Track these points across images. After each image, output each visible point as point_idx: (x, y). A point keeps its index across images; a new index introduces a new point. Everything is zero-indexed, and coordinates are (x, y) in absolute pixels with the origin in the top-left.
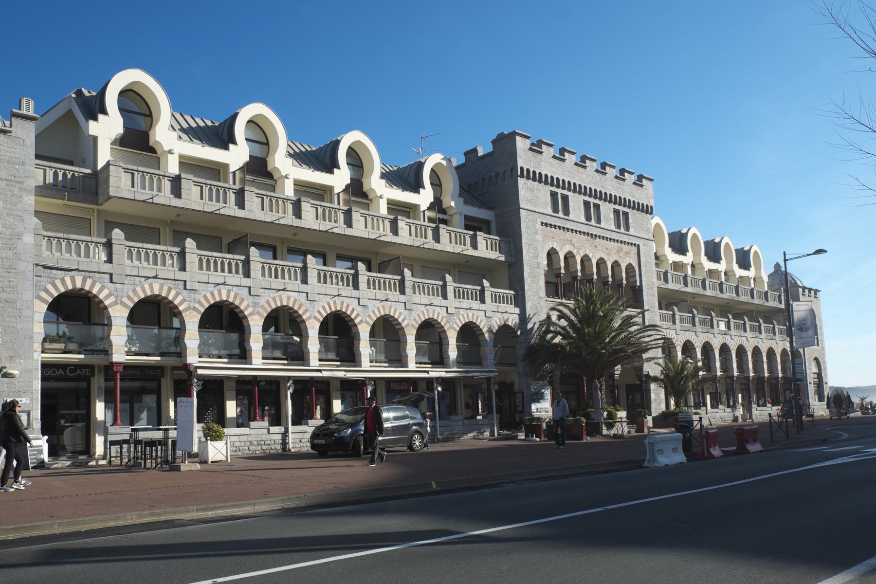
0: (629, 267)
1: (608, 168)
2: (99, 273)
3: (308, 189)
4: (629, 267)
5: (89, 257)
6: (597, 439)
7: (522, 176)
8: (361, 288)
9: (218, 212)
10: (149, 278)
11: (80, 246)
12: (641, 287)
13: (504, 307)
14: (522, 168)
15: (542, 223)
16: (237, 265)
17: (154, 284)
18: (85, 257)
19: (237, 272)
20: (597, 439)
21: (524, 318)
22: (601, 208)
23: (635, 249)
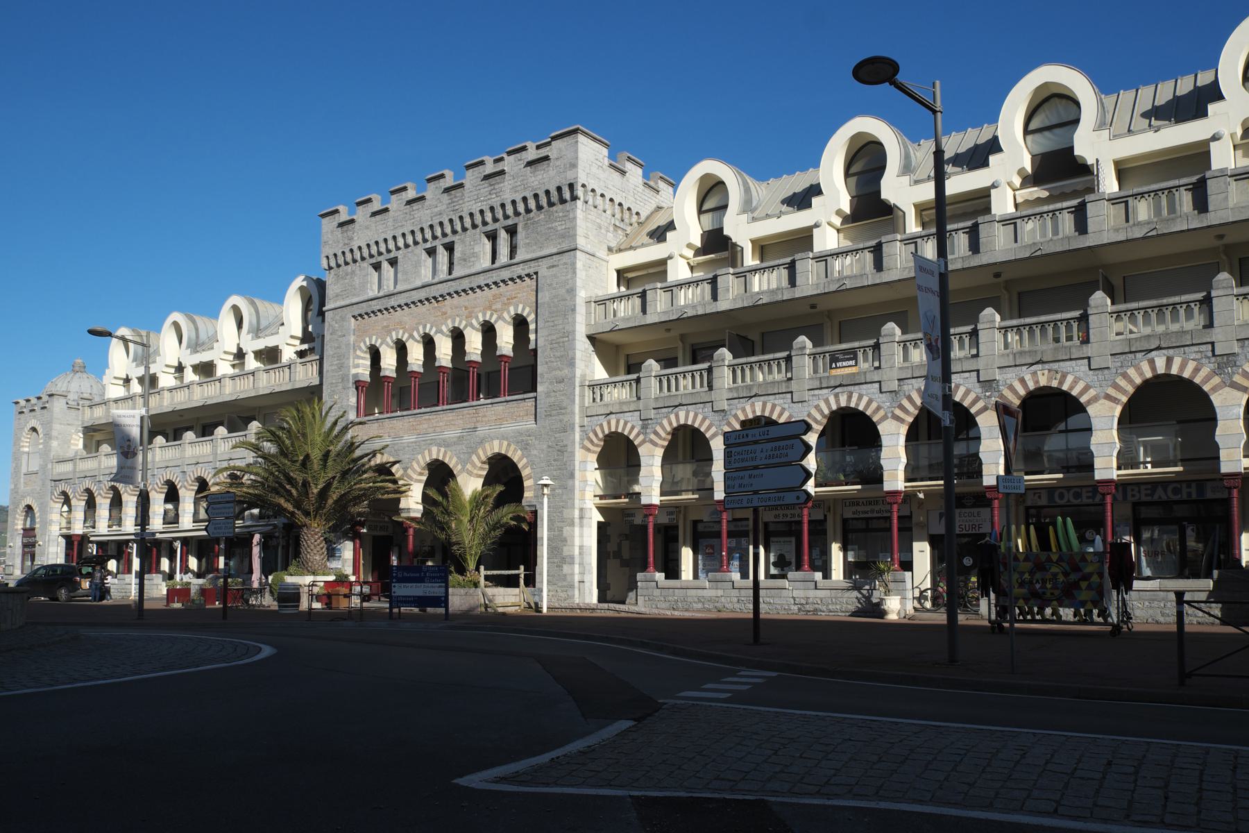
3: (651, 271)
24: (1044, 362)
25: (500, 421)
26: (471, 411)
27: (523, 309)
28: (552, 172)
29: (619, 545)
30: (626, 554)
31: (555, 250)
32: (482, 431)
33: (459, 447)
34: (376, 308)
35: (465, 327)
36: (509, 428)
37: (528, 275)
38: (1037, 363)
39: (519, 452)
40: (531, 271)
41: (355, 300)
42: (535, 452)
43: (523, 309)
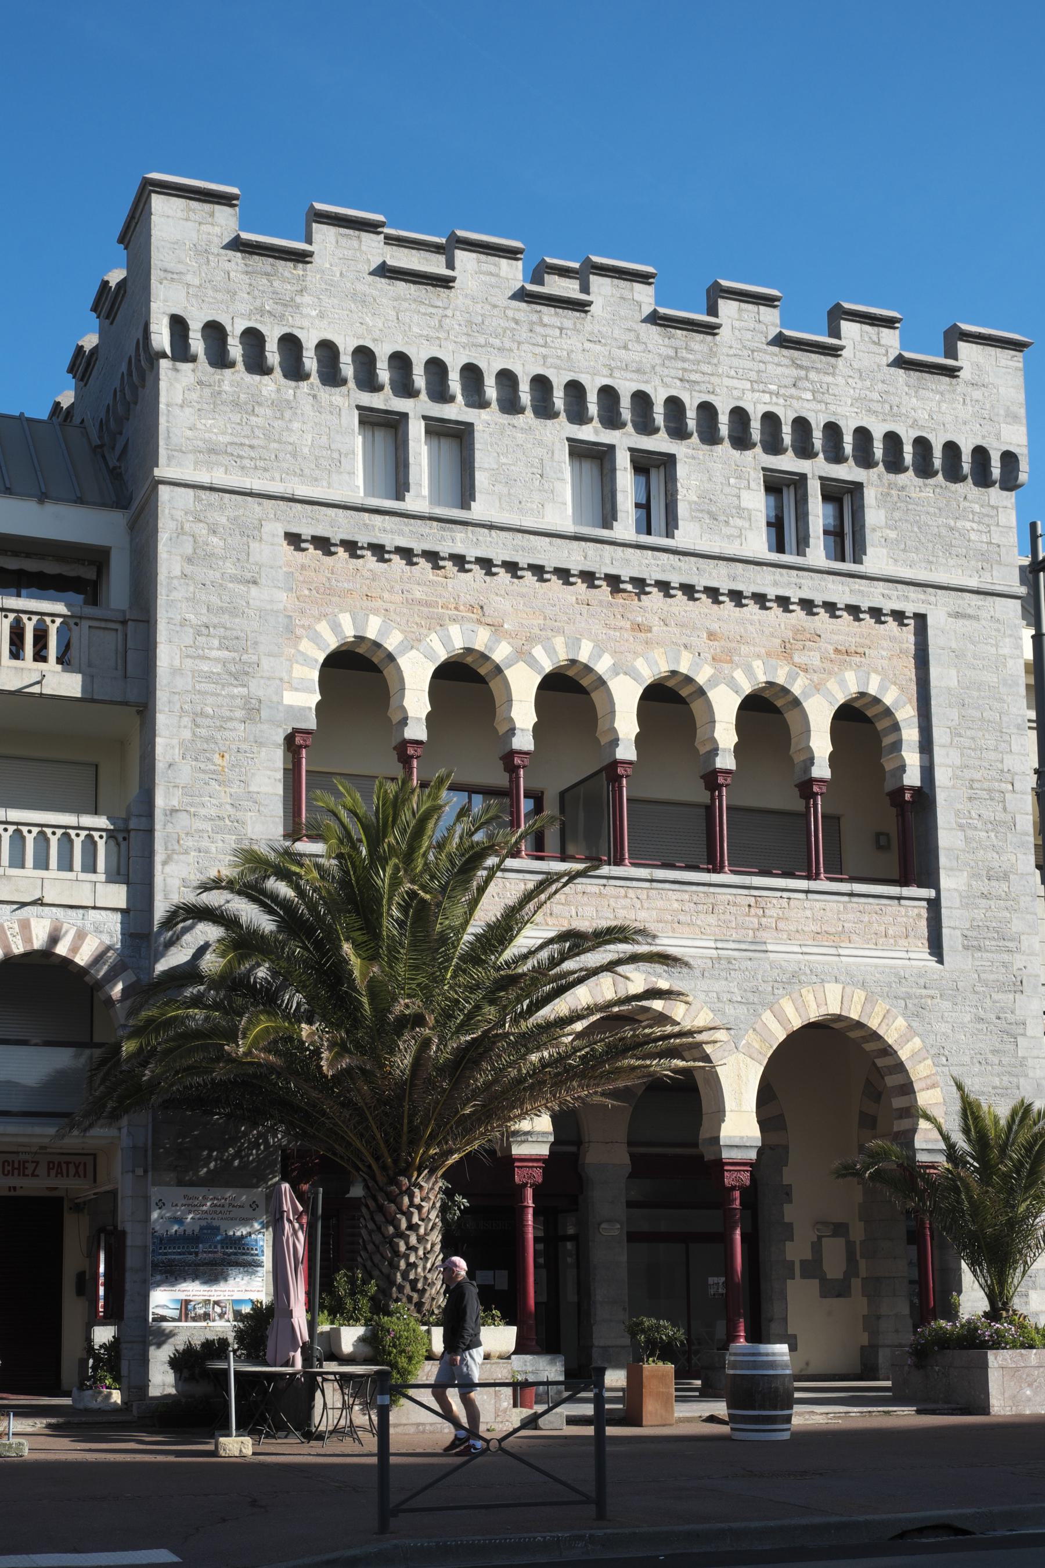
0: (858, 721)
1: (727, 308)
2: (94, 908)
4: (858, 721)
5: (71, 869)
6: (289, 1450)
7: (182, 352)
8: (51, 867)
9: (36, 689)
10: (23, 904)
11: (47, 840)
12: (924, 798)
13: (57, 885)
14: (179, 325)
15: (294, 539)
16: (90, 844)
17: (33, 922)
18: (84, 870)
19: (90, 866)
20: (289, 1450)
21: (141, 932)
22: (681, 471)
23: (908, 636)
24: (42, 904)
25: (839, 937)
26: (743, 898)
27: (336, 627)
28: (573, 342)
29: (817, 1247)
30: (834, 1267)
31: (973, 583)
32: (783, 951)
33: (719, 986)
34: (390, 541)
35: (714, 681)
36: (864, 957)
37: (899, 616)
38: (33, 903)
39: (901, 1022)
40: (910, 609)
41: (303, 491)
42: (944, 1028)
43: (336, 627)
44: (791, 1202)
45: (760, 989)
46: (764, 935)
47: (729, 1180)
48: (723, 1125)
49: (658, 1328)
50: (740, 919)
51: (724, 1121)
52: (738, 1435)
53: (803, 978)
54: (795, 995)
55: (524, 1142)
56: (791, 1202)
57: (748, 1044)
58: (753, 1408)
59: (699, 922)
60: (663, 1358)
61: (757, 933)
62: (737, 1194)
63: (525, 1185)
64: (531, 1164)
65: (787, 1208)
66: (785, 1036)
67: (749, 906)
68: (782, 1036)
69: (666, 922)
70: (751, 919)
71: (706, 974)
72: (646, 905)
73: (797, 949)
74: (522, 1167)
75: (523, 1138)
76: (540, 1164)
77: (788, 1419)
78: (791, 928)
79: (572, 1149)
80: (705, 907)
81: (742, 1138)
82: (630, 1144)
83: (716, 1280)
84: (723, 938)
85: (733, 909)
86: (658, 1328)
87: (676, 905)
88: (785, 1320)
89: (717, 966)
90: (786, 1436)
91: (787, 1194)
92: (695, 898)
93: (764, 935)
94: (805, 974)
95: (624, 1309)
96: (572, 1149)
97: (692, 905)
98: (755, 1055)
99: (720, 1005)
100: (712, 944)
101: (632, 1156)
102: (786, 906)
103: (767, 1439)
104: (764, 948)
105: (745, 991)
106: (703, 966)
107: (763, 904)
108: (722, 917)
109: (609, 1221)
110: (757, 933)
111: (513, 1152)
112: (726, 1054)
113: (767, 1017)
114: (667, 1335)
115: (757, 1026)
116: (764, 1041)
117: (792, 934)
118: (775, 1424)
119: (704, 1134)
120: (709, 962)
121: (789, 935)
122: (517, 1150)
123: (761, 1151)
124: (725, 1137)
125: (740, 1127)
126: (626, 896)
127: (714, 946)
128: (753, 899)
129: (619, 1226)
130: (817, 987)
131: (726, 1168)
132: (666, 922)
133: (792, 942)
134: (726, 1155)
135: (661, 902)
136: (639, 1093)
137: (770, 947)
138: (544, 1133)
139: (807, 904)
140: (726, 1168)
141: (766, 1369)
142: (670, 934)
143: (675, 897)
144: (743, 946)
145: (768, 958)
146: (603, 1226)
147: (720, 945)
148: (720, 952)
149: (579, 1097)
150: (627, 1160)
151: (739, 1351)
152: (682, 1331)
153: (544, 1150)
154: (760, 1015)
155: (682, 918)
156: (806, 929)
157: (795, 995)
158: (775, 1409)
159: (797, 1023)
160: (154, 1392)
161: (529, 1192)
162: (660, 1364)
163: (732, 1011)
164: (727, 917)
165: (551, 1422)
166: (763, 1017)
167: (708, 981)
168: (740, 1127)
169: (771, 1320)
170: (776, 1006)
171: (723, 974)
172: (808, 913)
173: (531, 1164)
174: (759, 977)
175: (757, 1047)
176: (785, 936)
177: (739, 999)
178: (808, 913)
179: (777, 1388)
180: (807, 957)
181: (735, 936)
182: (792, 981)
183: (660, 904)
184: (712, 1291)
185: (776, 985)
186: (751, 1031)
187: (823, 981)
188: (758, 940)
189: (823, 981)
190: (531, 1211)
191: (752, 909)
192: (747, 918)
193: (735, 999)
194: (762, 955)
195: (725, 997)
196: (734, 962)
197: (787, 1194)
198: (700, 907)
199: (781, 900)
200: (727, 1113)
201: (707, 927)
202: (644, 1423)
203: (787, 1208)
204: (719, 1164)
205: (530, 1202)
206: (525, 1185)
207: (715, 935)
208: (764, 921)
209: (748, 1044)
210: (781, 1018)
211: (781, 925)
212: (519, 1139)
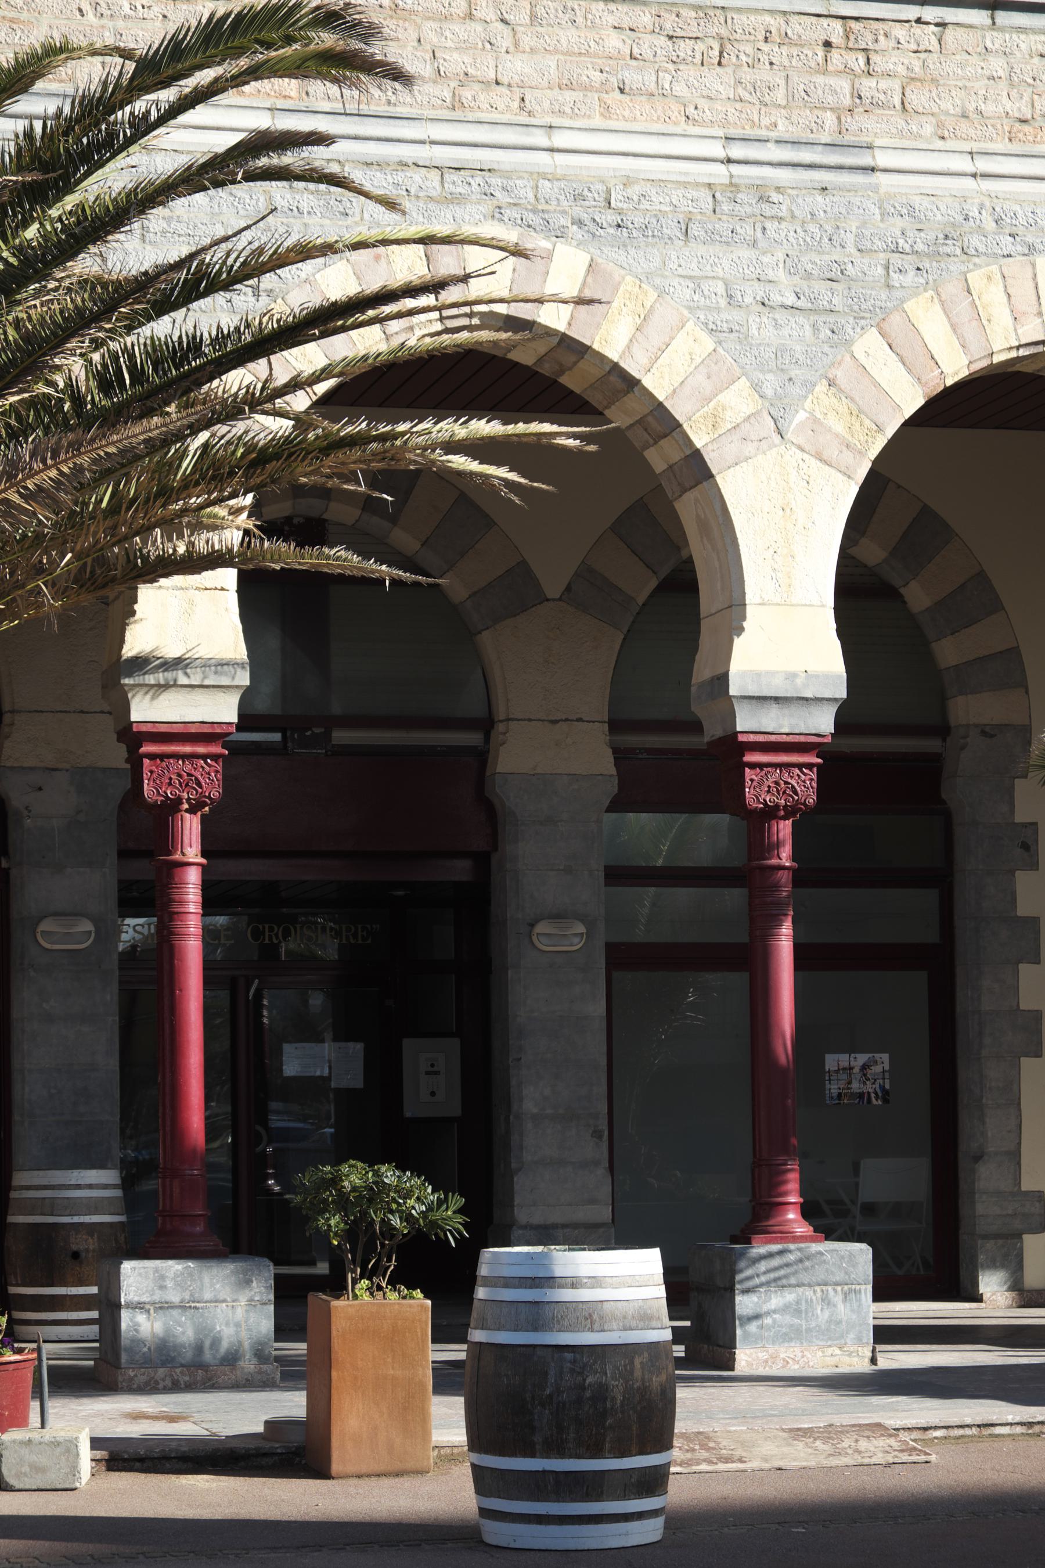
44: (1034, 866)
45: (850, 270)
46: (866, 126)
47: (758, 790)
48: (739, 644)
49: (375, 1193)
50: (799, 82)
51: (741, 630)
52: (496, 1532)
53: (976, 242)
54: (952, 288)
55: (165, 687)
56: (1034, 866)
57: (815, 423)
58: (529, 1452)
59: (680, 89)
60: (405, 1278)
61: (847, 119)
62: (785, 828)
63: (172, 806)
64: (187, 749)
65: (1023, 879)
66: (920, 402)
67: (828, 44)
68: (912, 402)
69: (586, 88)
70: (832, 81)
71: (695, 230)
72: (527, 41)
73: (964, 164)
74: (162, 757)
75: (161, 677)
76: (217, 749)
77: (654, 1481)
78: (947, 105)
79: (472, 738)
80: (700, 46)
81: (791, 676)
82: (616, 726)
83: (844, 1059)
84: (749, 132)
85: (780, 55)
86: (375, 1193)
87: (614, 42)
88: (1015, 1156)
89: (726, 207)
90: (650, 1531)
91: (1025, 847)
92: (669, 22)
93: (866, 126)
94: (980, 230)
95: (597, 1134)
96: (472, 738)
97: (663, 41)
98: (832, 452)
99: (736, 315)
100: (717, 150)
101: (621, 755)
102: (934, 45)
103: (572, 1545)
104: (866, 160)
105: (808, 276)
106: (685, 206)
107: (866, 40)
108: (747, 75)
109: (558, 916)
110: (847, 119)
111: (134, 717)
112: (750, 448)
113: (869, 345)
114: (408, 1218)
115: (839, 375)
116: (858, 413)
117: (950, 123)
118: (599, 1498)
119: (702, 672)
120: (705, 196)
121: (940, 125)
122: (145, 710)
123: (847, 719)
124: (743, 674)
125: (785, 649)
126: (470, 16)
127: (721, 154)
128: (837, 25)
129: (581, 929)
130: (1012, 266)
131: (749, 758)
132: (586, 88)
133: (950, 145)
134: (748, 722)
135: (572, 32)
136: (641, 599)
137: (883, 159)
138: (222, 664)
139: (994, 40)
140: (749, 758)
141: (570, 1329)
142: (597, 122)
143: (611, 20)
144: (806, 156)
145: (875, 189)
146: (541, 928)
147: (737, 151)
148: (735, 169)
149: (40, 488)
150: (607, 764)
151: (507, 1272)
152: (457, 1201)
153: (224, 710)
154: (848, 343)
155: (632, 77)
156: (989, 108)
157: (952, 288)
158: (596, 1452)
159: (955, 368)
160: (327, 1271)
161: (191, 829)
162: (393, 1296)
163: (769, 333)
164: (763, 74)
165: (37, 1469)
166: (858, 349)
167: (702, 250)
168: (785, 649)
169: (978, 1158)
170: (896, 319)
171: (746, 230)
172: (997, 65)
173: (187, 749)
174: (850, 239)
175: (839, 428)
176: (928, 129)
177: (791, 300)
178: (997, 65)
179: (602, 1392)
180: (987, 185)
181: (783, 129)
182: (941, 249)
183: (568, 37)
184: (833, 1088)
185: (896, 260)
186: (822, 387)
187: (1031, 249)
188: (849, 139)
189: (1031, 249)
190: (193, 877)
191: (835, 54)
192: (820, 80)
193: (776, 299)
194: (859, 179)
195: (751, 292)
196: (775, 197)
197: (1025, 847)
198: (685, 48)
199: (917, 29)
200: (749, 610)
201: (703, 103)
202: (336, 1467)
203: (1023, 879)
204: (732, 749)
205: (192, 852)
206: (172, 806)
207: (725, 123)
208: (868, 85)
209: (815, 423)
210: (908, 352)
211: (917, 98)
212: (151, 679)
